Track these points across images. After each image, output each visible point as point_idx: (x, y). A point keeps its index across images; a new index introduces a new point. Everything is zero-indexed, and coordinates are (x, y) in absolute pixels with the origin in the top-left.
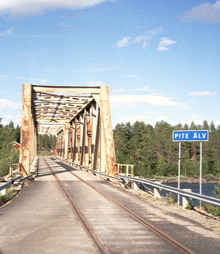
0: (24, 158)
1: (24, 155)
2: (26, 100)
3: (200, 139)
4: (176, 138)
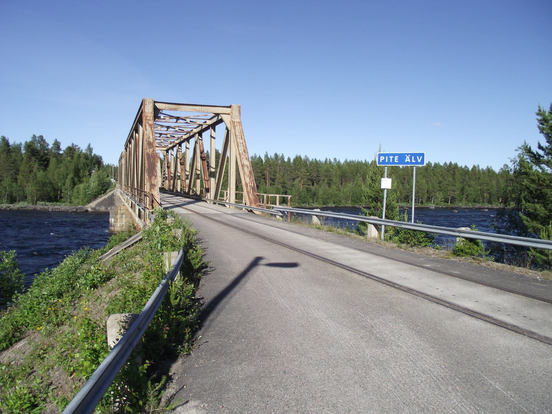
0: (152, 187)
1: (151, 182)
2: (148, 118)
3: (414, 163)
4: (381, 161)
